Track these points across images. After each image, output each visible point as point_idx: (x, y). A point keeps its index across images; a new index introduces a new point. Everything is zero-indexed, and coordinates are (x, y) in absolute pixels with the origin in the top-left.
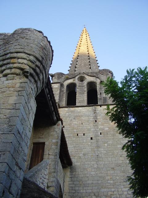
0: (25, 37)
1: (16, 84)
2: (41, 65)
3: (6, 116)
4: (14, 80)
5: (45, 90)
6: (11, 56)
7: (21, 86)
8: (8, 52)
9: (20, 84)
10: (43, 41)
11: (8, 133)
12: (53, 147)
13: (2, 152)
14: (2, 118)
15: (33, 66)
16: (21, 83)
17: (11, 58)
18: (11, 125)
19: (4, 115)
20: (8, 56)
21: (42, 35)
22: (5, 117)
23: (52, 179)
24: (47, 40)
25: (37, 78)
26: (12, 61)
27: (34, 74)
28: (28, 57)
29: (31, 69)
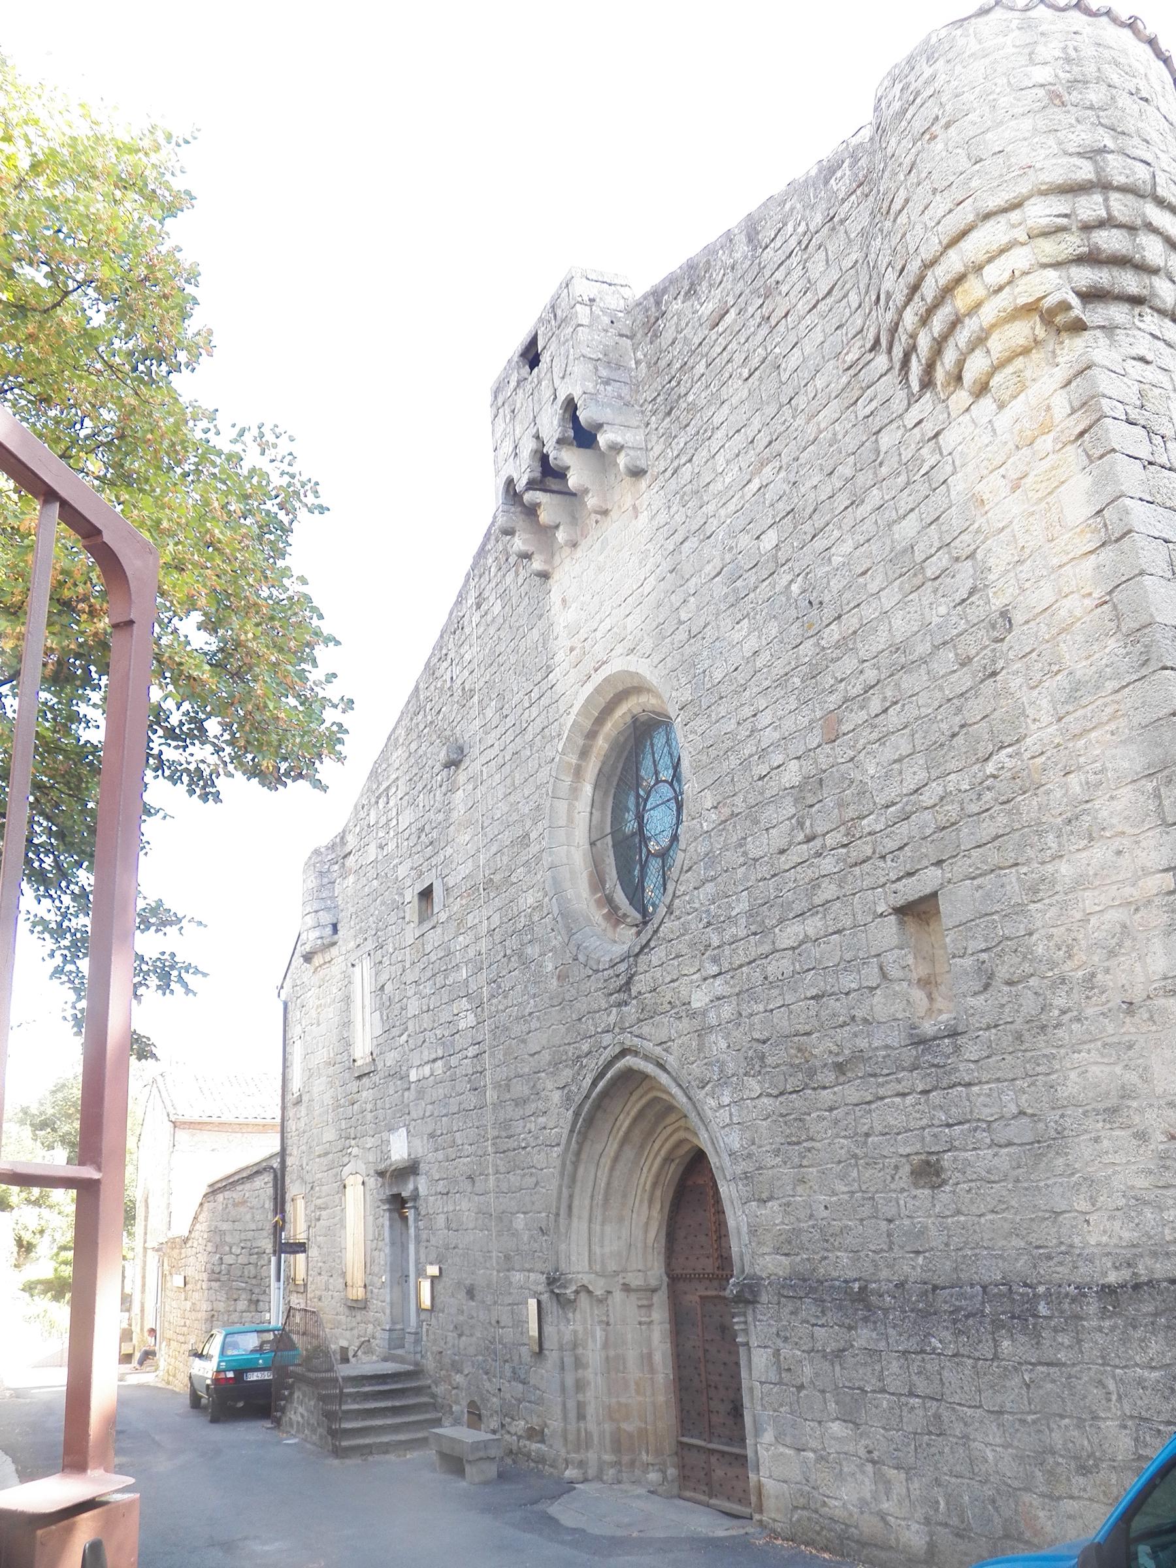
1: (1048, 408)
2: (1106, 200)
3: (1090, 594)
4: (1029, 391)
7: (1076, 404)
8: (914, 267)
11: (1139, 675)
13: (1159, 775)
14: (1079, 615)
15: (1072, 244)
16: (1069, 383)
17: (947, 292)
19: (1084, 596)
20: (929, 290)
22: (1087, 601)
25: (1130, 282)
26: (961, 300)
28: (1013, 226)
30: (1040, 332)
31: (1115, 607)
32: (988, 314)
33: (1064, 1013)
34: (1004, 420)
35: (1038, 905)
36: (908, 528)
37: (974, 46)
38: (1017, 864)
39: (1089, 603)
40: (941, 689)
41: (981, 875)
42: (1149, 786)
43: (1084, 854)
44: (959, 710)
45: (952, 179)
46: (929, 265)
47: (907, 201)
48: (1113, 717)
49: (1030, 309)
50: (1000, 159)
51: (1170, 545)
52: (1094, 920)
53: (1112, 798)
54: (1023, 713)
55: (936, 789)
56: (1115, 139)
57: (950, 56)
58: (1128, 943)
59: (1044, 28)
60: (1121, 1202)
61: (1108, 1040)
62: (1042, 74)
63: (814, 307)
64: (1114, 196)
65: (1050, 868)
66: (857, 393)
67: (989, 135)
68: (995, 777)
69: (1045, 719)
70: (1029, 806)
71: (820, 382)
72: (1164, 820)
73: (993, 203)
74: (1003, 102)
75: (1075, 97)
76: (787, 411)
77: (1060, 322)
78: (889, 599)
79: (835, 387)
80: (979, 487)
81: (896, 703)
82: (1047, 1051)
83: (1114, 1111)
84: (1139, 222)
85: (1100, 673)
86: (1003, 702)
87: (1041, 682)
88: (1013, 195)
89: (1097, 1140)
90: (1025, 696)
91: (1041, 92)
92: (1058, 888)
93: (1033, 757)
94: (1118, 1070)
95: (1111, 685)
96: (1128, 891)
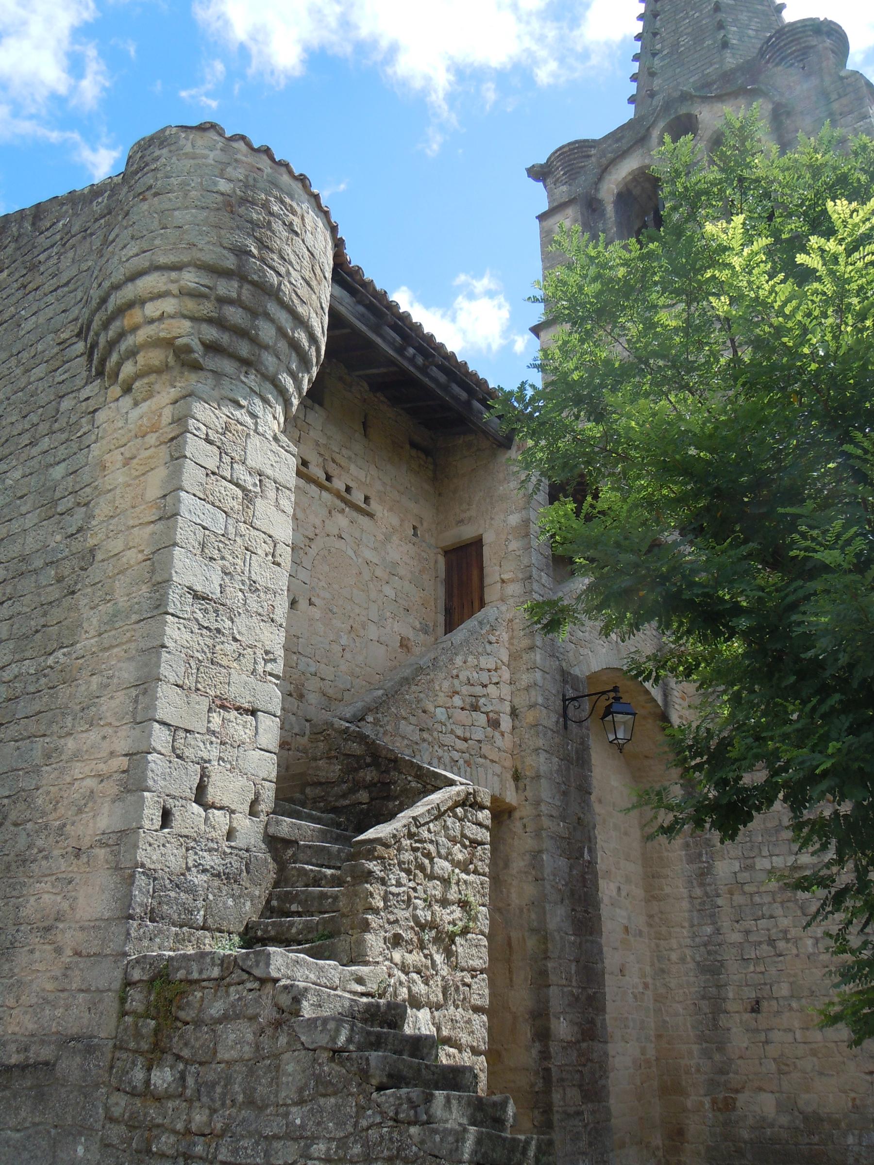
0: (150, 188)
2: (241, 287)
4: (154, 399)
5: (379, 341)
6: (119, 302)
7: (176, 418)
8: (106, 284)
9: (171, 407)
10: (229, 169)
12: (514, 545)
15: (207, 308)
17: (121, 311)
18: (159, 583)
20: (111, 305)
21: (217, 138)
23: (525, 679)
24: (253, 149)
25: (244, 349)
26: (127, 321)
27: (225, 339)
28: (172, 282)
29: (204, 327)
30: (171, 360)
31: (153, 563)
32: (142, 335)
33: (40, 851)
34: (134, 414)
35: (48, 768)
36: (58, 472)
37: (188, 149)
38: (44, 735)
39: (141, 557)
40: (39, 595)
41: (22, 739)
42: (134, 692)
43: (84, 735)
44: (45, 615)
45: (145, 233)
46: (116, 287)
47: (117, 236)
48: (129, 641)
49: (168, 343)
50: (178, 232)
51: (207, 532)
52: (77, 784)
53: (112, 697)
54: (81, 626)
55: (15, 669)
56: (260, 249)
57: (173, 148)
58: (90, 805)
59: (239, 156)
60: (34, 1000)
61: (60, 876)
62: (224, 186)
63: (55, 290)
64: (246, 286)
65: (62, 741)
66: (58, 363)
67: (177, 213)
68: (52, 668)
69: (92, 633)
70: (64, 691)
71: (40, 347)
72: (135, 719)
73: (162, 260)
74: (193, 193)
75: (242, 210)
76: (13, 361)
77: (184, 360)
78: (30, 520)
79: (47, 355)
80: (107, 457)
81: (10, 599)
82: (21, 880)
83: (48, 929)
84: (261, 310)
85: (131, 607)
86: (72, 614)
87: (98, 605)
88: (177, 259)
89: (32, 951)
90: (86, 612)
91: (220, 198)
92: (63, 757)
93: (77, 659)
94: (59, 898)
95: (135, 617)
96: (102, 766)
